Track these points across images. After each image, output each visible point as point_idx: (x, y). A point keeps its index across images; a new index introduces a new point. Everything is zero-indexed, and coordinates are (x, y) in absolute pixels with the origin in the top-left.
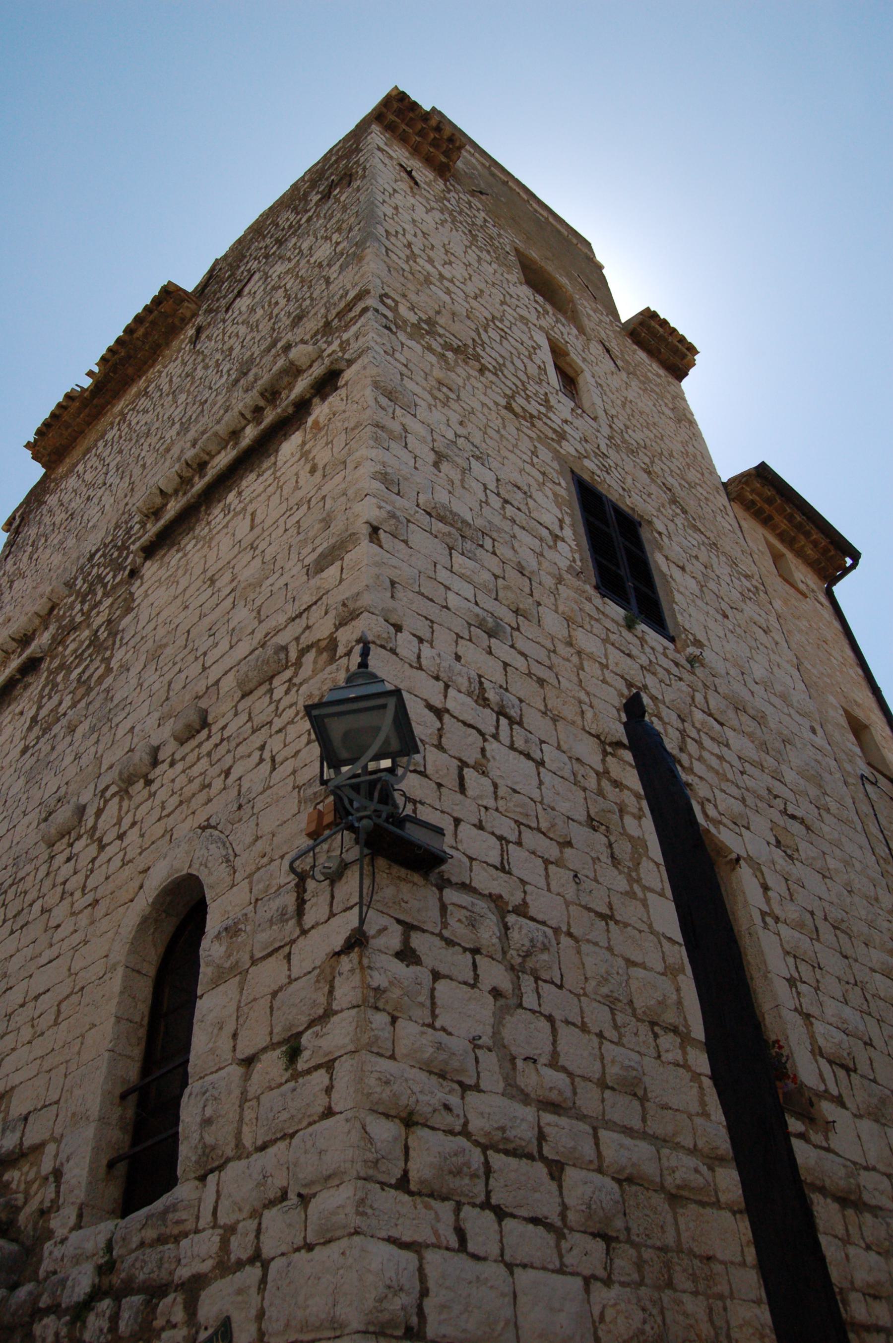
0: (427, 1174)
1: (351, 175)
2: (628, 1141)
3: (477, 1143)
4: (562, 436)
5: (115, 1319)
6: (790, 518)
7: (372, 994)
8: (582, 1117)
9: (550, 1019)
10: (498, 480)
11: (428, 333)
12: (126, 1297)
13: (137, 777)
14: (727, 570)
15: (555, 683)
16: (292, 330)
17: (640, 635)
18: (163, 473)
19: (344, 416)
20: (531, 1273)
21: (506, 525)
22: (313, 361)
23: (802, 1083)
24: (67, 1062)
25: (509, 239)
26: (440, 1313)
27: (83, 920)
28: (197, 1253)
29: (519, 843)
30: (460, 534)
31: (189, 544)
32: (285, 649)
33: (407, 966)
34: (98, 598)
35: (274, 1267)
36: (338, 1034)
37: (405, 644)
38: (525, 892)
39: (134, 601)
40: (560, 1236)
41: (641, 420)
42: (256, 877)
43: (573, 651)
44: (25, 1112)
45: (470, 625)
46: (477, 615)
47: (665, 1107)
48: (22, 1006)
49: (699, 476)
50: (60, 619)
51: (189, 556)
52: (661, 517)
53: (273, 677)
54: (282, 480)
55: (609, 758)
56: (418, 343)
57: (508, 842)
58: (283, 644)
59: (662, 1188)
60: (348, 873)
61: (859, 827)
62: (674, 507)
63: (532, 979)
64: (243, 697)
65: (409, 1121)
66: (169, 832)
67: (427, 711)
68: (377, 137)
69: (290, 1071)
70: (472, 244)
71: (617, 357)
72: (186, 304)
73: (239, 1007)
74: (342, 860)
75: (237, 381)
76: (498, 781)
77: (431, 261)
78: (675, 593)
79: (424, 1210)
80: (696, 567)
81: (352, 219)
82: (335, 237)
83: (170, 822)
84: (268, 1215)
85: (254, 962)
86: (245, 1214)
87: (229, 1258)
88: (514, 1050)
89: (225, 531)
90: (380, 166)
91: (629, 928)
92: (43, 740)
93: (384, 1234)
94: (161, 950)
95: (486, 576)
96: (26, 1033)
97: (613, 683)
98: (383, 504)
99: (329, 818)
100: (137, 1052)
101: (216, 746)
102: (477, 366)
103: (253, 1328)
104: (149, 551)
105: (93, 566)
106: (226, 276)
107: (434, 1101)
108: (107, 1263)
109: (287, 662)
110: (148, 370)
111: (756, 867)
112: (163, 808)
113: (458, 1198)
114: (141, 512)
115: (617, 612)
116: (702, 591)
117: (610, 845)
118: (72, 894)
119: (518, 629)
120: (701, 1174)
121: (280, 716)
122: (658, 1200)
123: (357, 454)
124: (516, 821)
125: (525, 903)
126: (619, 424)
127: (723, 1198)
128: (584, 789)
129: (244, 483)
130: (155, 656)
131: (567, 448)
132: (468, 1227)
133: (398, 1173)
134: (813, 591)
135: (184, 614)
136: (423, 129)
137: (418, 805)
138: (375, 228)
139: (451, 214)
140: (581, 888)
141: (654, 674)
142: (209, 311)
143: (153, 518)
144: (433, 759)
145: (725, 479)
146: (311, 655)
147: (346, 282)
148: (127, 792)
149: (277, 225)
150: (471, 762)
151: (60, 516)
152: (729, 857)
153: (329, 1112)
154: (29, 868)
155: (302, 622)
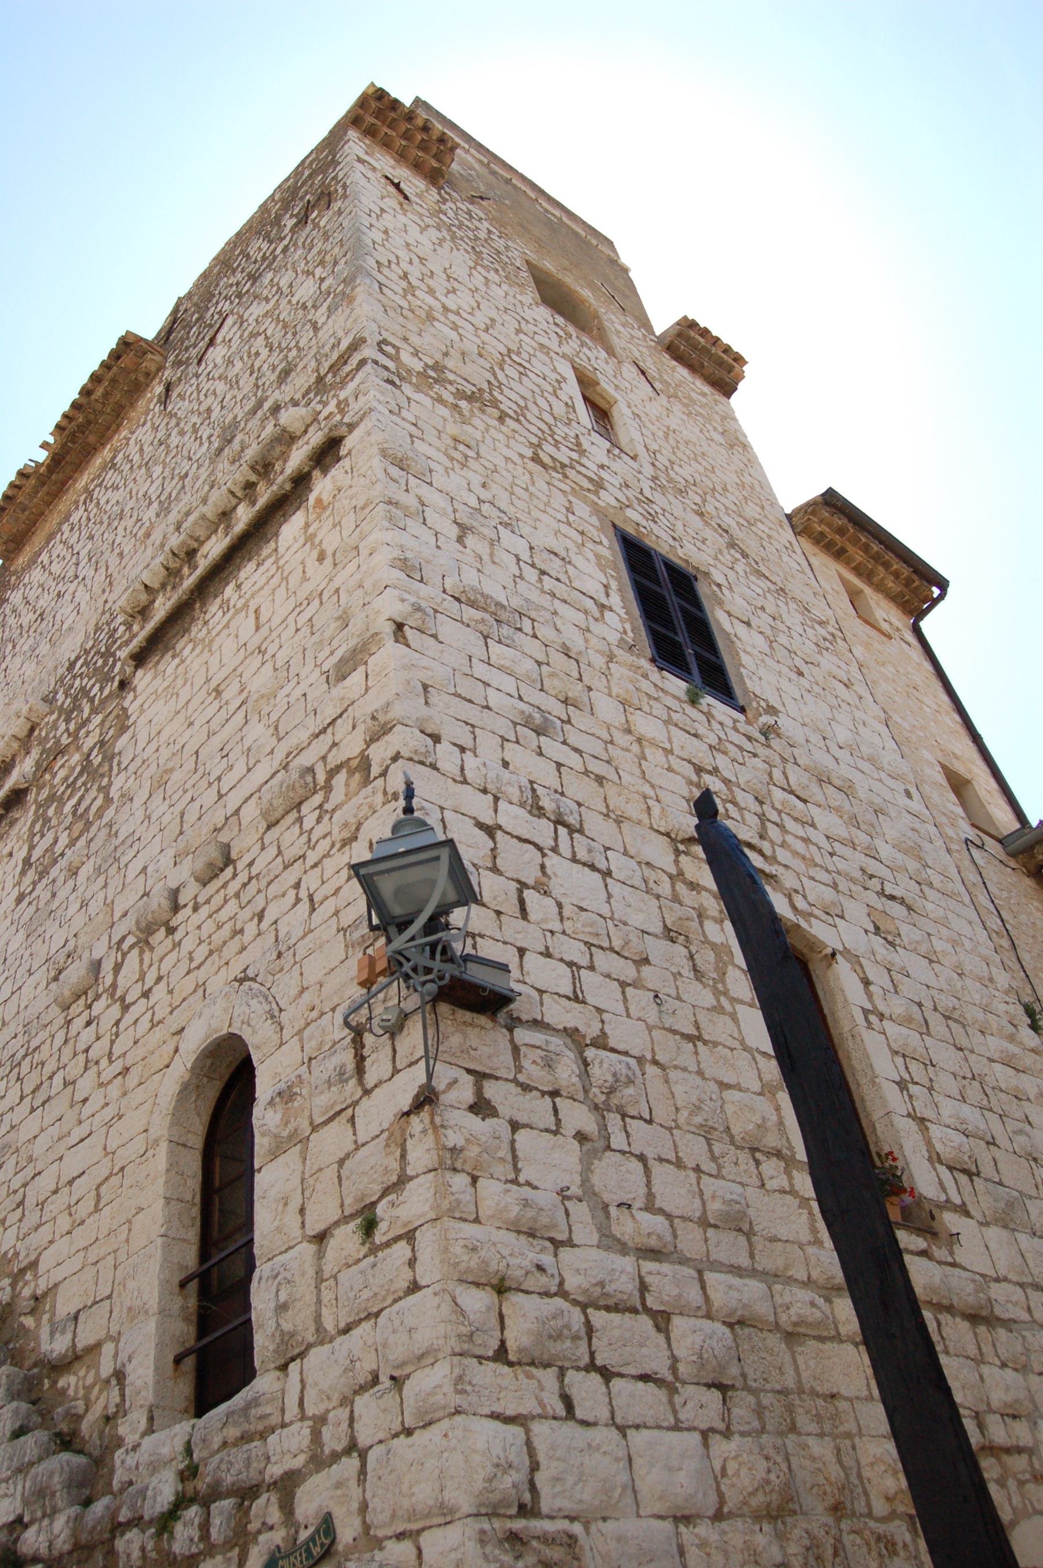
0: (526, 1341)
1: (329, 194)
2: (736, 1281)
3: (575, 1303)
4: (599, 485)
5: (205, 1527)
6: (866, 548)
7: (448, 1155)
8: (683, 1261)
9: (642, 1158)
10: (531, 548)
11: (436, 381)
12: (215, 1501)
13: (157, 925)
14: (799, 618)
15: (616, 778)
16: (279, 388)
17: (705, 710)
18: (145, 564)
19: (350, 492)
20: (645, 1432)
21: (545, 601)
22: (308, 426)
23: (921, 1195)
24: (115, 1251)
25: (519, 251)
26: (554, 1486)
27: (114, 1090)
28: (287, 1450)
29: (592, 968)
30: (495, 618)
31: (184, 646)
32: (311, 770)
33: (483, 1119)
34: (85, 715)
35: (372, 1456)
36: (416, 1202)
37: (446, 756)
38: (603, 1022)
39: (128, 717)
40: (672, 1390)
41: (688, 452)
42: (306, 1033)
43: (631, 738)
44: (73, 1311)
45: (515, 724)
46: (523, 712)
47: (774, 1239)
48: (55, 1192)
49: (759, 509)
50: (42, 741)
51: (188, 662)
52: (719, 566)
53: (300, 803)
54: (287, 569)
55: (683, 858)
56: (427, 395)
57: (579, 967)
58: (309, 765)
59: (777, 1327)
60: (409, 1023)
61: (967, 899)
62: (732, 551)
63: (619, 1117)
64: (269, 827)
65: (501, 1289)
66: (201, 987)
67: (477, 831)
68: (355, 145)
69: (368, 1245)
70: (476, 263)
71: (654, 378)
72: (150, 356)
73: (303, 1180)
74: (401, 1011)
75: (220, 451)
76: (562, 900)
77: (431, 292)
78: (742, 654)
79: (526, 1381)
80: (762, 621)
81: (337, 250)
82: (318, 272)
83: (201, 975)
84: (360, 1401)
85: (315, 1128)
86: (335, 1402)
87: (322, 1451)
88: (606, 1197)
89: (226, 632)
90: (363, 182)
91: (720, 1047)
92: (40, 886)
93: (486, 1411)
94: (206, 1118)
95: (529, 665)
96: (64, 1222)
97: (679, 770)
98: (406, 596)
99: (381, 965)
100: (193, 1235)
101: (245, 885)
102: (496, 413)
103: (357, 1522)
104: (140, 658)
105: (74, 677)
106: (193, 319)
107: (526, 1263)
108: (188, 1467)
109: (315, 786)
110: (111, 438)
111: (855, 960)
112: (191, 959)
113: (560, 1364)
114: (125, 612)
115: (677, 686)
116: (771, 647)
117: (692, 957)
118: (97, 1063)
119: (569, 722)
120: (818, 1308)
121: (314, 848)
122: (774, 1340)
123: (371, 539)
124: (586, 943)
125: (604, 1034)
126: (662, 460)
127: (843, 1330)
128: (658, 897)
129: (243, 574)
130: (161, 782)
131: (607, 499)
132: (574, 1392)
133: (495, 1344)
134: (898, 630)
135: (189, 732)
136: (408, 130)
137: (478, 939)
138: (365, 261)
139: (449, 230)
140: (663, 1009)
141: (725, 753)
142: (178, 363)
143: (139, 617)
144: (488, 885)
145: (788, 511)
146: (341, 778)
147: (337, 328)
148: (147, 943)
149: (248, 257)
150: (531, 882)
151: (27, 618)
152: (824, 952)
153: (415, 1287)
154: (43, 1035)
155: (327, 739)
